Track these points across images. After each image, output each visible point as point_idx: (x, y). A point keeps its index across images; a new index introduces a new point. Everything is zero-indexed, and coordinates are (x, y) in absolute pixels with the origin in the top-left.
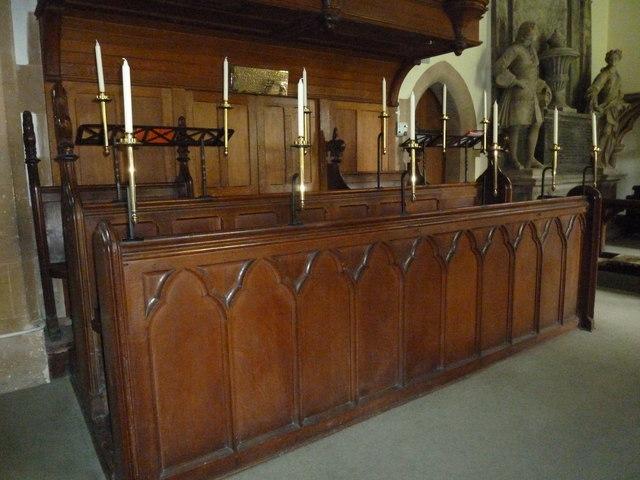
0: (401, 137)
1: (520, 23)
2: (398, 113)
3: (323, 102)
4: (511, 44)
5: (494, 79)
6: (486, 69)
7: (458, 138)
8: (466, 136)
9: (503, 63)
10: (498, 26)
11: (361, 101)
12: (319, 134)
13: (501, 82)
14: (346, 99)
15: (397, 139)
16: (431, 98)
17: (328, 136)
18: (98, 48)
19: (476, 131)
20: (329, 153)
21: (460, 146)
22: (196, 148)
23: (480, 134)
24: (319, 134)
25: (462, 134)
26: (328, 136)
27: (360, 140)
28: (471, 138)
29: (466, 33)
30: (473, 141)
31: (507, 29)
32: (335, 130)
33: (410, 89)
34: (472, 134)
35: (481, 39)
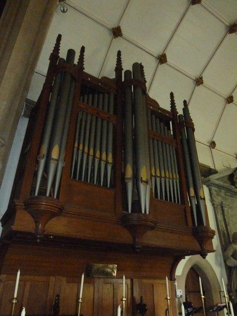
0: (179, 298)
1: (232, 233)
2: (176, 284)
3: (135, 280)
4: (230, 243)
5: (225, 261)
6: (220, 256)
7: (212, 308)
8: (216, 306)
9: (228, 254)
10: (222, 233)
11: (155, 278)
12: (133, 298)
13: (229, 264)
14: (147, 278)
15: (177, 299)
16: (195, 273)
17: (138, 301)
18: (19, 273)
19: (222, 303)
20: (139, 311)
21: (213, 311)
22: (29, 98)
23: (224, 304)
24: (133, 298)
25: (215, 304)
26: (138, 301)
27: (155, 301)
28: (219, 307)
29: (206, 247)
30: (221, 308)
31: (226, 235)
32: (142, 297)
33: (182, 268)
34: (219, 305)
35: (215, 248)
